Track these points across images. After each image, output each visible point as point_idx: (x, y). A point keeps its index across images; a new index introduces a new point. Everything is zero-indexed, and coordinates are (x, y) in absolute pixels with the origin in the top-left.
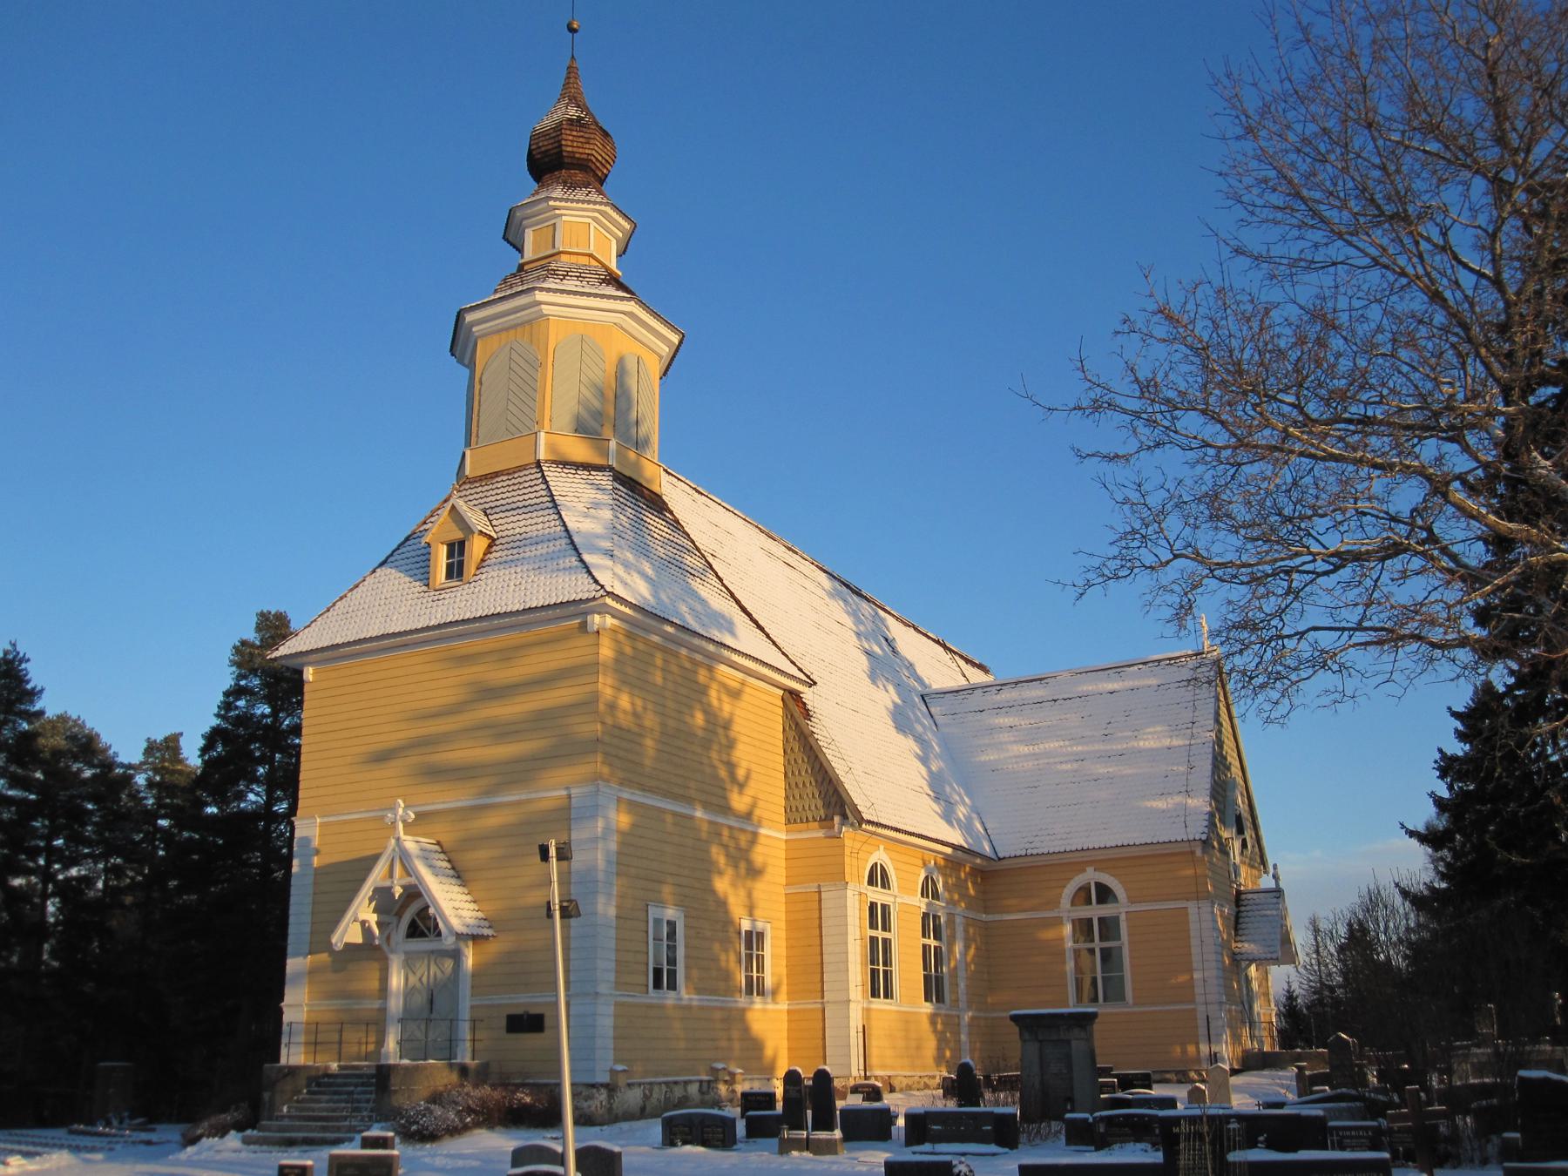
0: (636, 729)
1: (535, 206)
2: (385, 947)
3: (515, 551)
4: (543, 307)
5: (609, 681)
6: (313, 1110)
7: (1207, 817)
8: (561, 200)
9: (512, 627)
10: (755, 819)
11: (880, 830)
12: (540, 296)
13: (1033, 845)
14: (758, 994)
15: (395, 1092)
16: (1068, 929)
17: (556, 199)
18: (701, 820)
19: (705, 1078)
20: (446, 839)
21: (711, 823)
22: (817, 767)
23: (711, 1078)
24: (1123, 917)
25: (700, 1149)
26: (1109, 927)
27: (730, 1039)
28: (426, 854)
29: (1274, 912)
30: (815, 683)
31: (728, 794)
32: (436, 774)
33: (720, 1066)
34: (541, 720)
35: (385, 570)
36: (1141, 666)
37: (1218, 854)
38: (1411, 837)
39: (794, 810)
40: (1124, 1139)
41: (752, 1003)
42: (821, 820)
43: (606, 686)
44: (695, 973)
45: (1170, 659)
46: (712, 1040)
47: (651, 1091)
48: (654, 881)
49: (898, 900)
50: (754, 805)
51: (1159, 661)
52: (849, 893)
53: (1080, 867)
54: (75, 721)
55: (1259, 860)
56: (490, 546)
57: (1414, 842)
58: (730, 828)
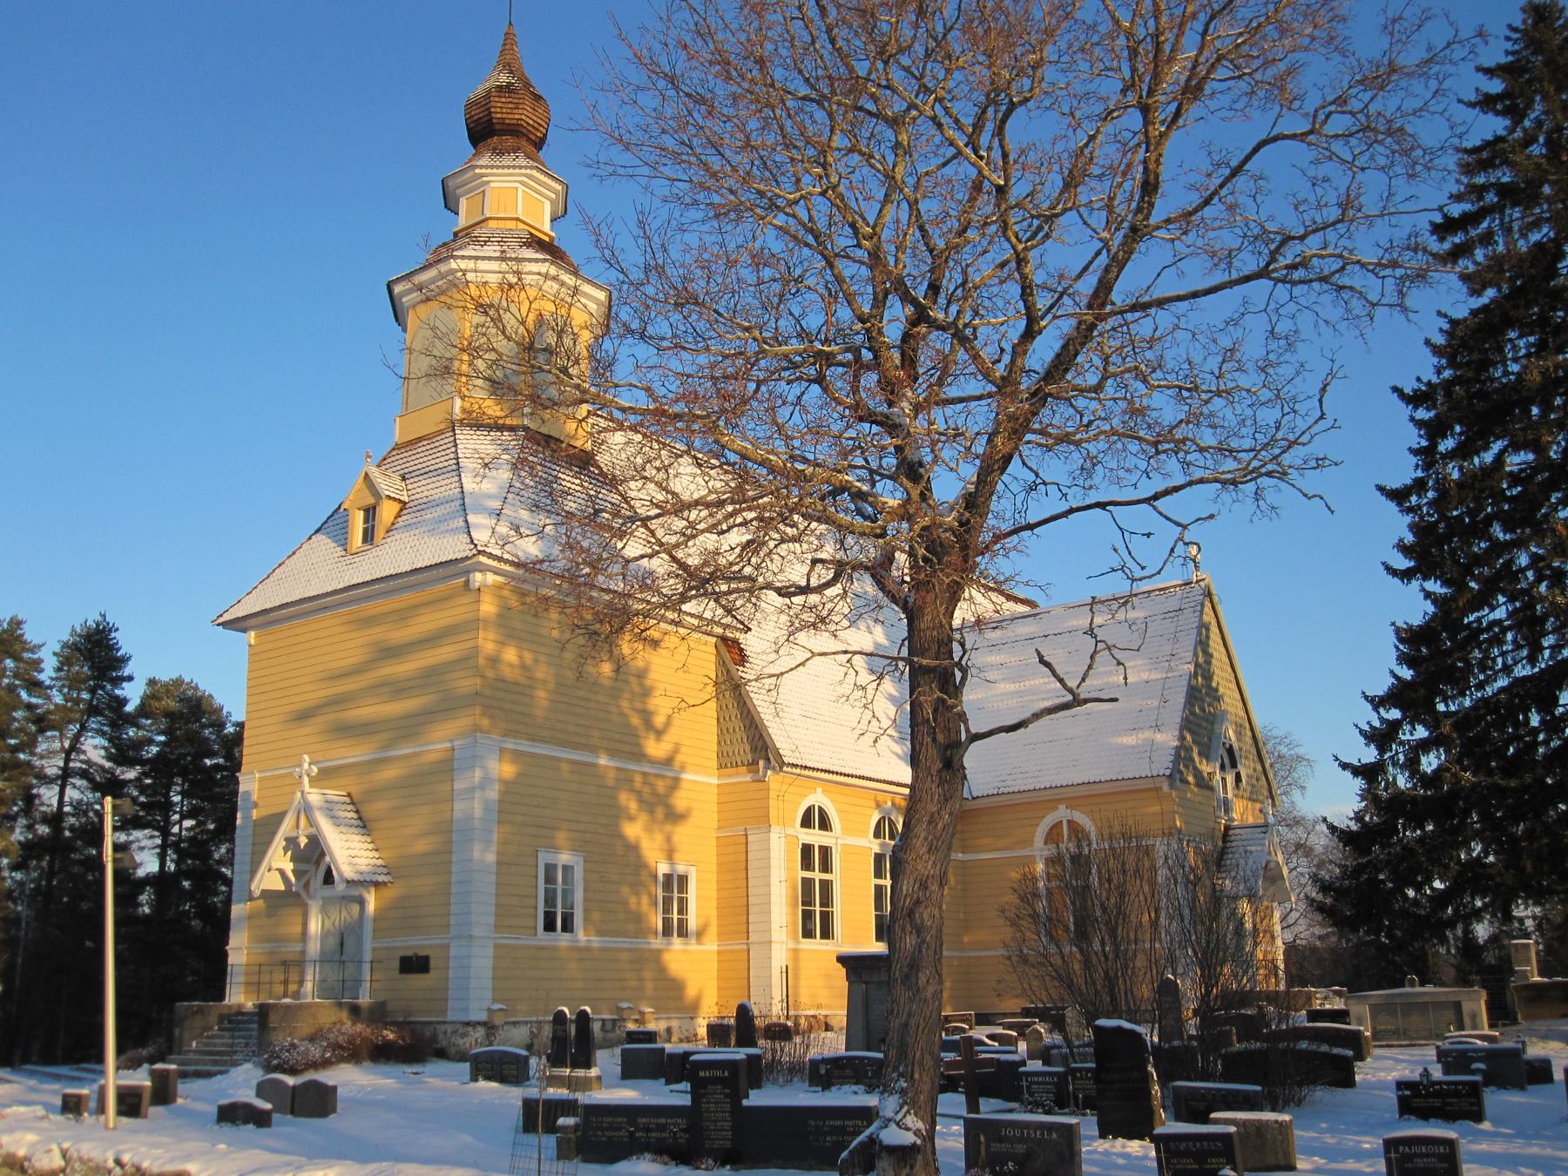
0: (524, 681)
2: (303, 893)
3: (418, 514)
5: (491, 635)
6: (215, 1045)
7: (1173, 752)
8: (487, 167)
9: (410, 587)
10: (677, 764)
11: (807, 772)
12: (453, 264)
14: (679, 935)
15: (275, 1028)
17: (481, 167)
18: (606, 767)
19: (606, 1016)
20: (354, 790)
21: (618, 769)
22: (745, 714)
23: (615, 1017)
25: (494, 1084)
27: (641, 979)
28: (330, 806)
29: (1259, 848)
30: (750, 629)
31: (642, 741)
32: (346, 731)
33: (625, 1005)
34: (430, 676)
35: (319, 536)
37: (1196, 790)
38: (1344, 769)
40: (844, 1080)
41: (670, 944)
42: (749, 764)
43: (487, 642)
44: (596, 916)
45: (1160, 590)
46: (619, 980)
47: (539, 1029)
48: (547, 828)
49: (840, 842)
50: (676, 751)
51: (1149, 592)
52: (774, 836)
53: (1052, 804)
54: (188, 684)
55: (1266, 793)
56: (401, 510)
57: (1348, 774)
58: (645, 774)
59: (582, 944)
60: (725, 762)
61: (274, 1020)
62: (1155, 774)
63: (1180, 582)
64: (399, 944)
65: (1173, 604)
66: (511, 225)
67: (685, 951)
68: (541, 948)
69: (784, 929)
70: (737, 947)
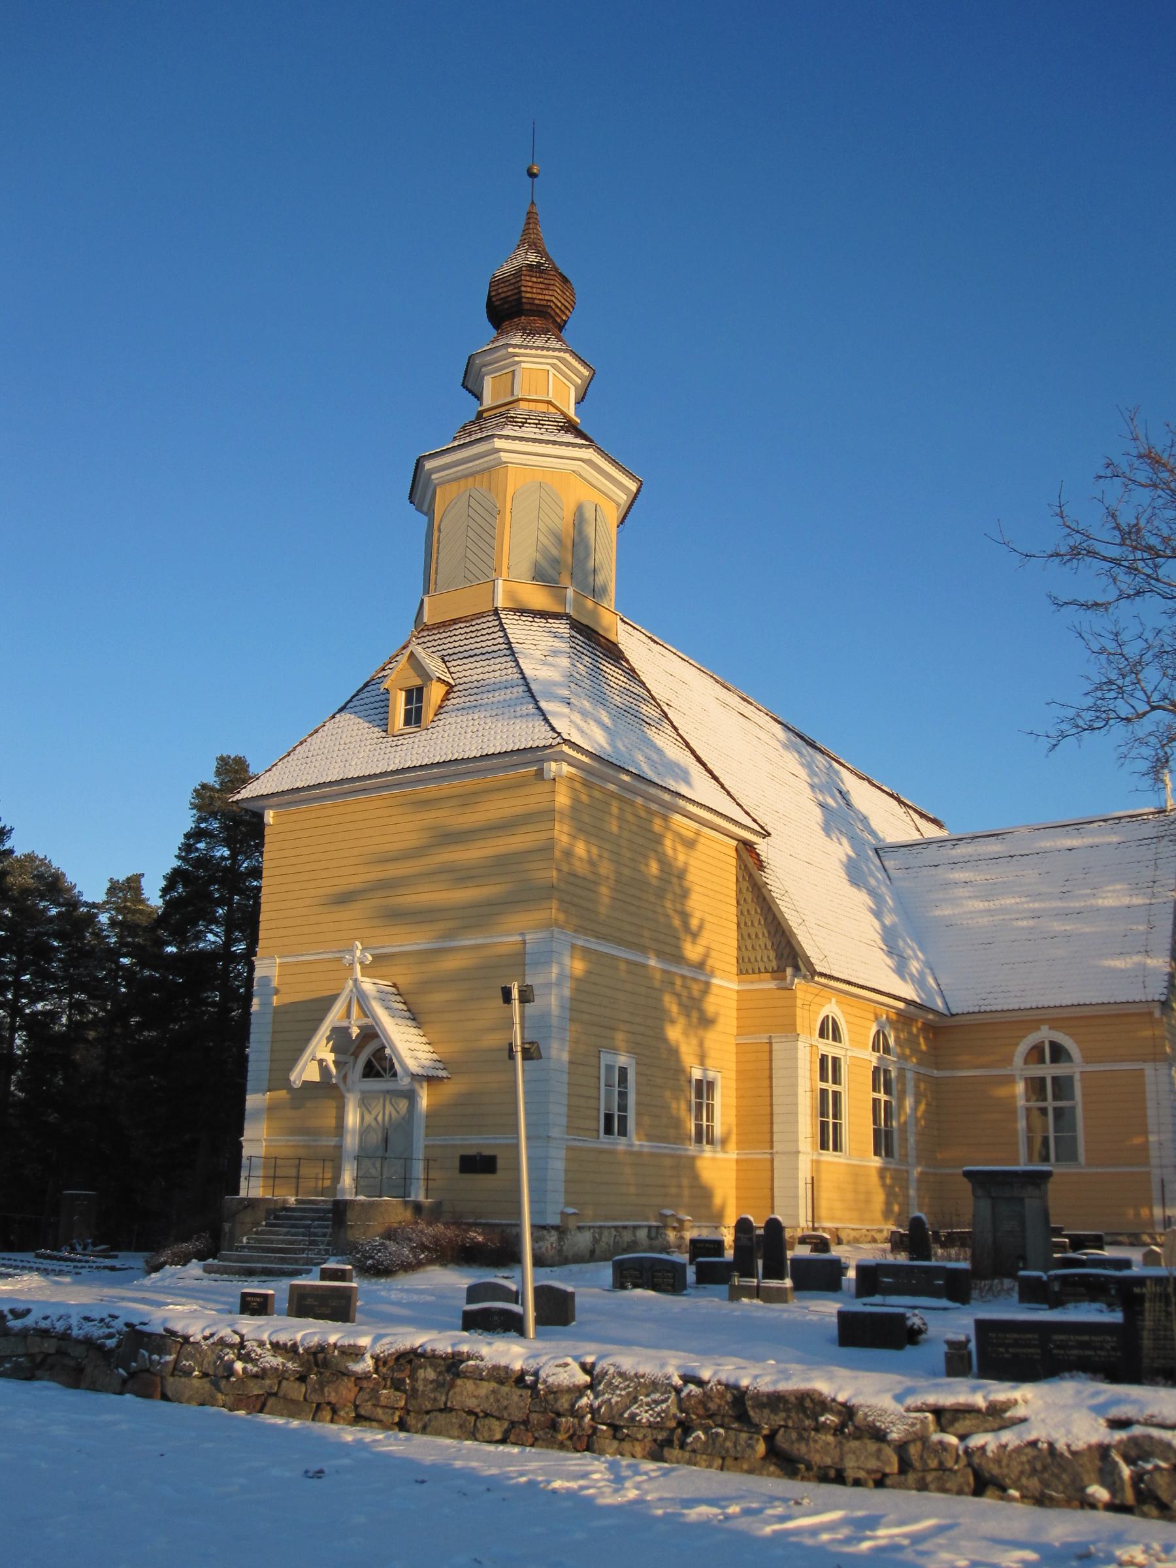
0: (590, 876)
1: (496, 352)
2: (341, 1086)
4: (502, 454)
6: (272, 1242)
7: (1166, 978)
8: (520, 347)
11: (832, 983)
12: (498, 443)
13: (985, 1002)
14: (708, 1143)
16: (1020, 1088)
17: (515, 346)
19: (654, 1224)
20: (400, 981)
21: (664, 971)
22: (770, 920)
24: (1077, 1077)
25: (651, 1293)
26: (1062, 1086)
27: (680, 1186)
30: (769, 834)
33: (668, 1212)
34: (502, 864)
35: (341, 718)
36: (1101, 823)
39: (746, 960)
40: (1078, 1298)
43: (562, 833)
44: (646, 1120)
47: (601, 1234)
51: (1120, 818)
52: (800, 1045)
54: (41, 860)
56: (448, 693)
58: (683, 977)
59: (635, 1149)
60: (745, 967)
61: (351, 1218)
62: (1150, 999)
63: (1152, 810)
64: (458, 1142)
65: (1148, 830)
66: (543, 407)
67: (713, 1159)
68: (602, 1151)
69: (809, 1140)
70: (760, 1156)
